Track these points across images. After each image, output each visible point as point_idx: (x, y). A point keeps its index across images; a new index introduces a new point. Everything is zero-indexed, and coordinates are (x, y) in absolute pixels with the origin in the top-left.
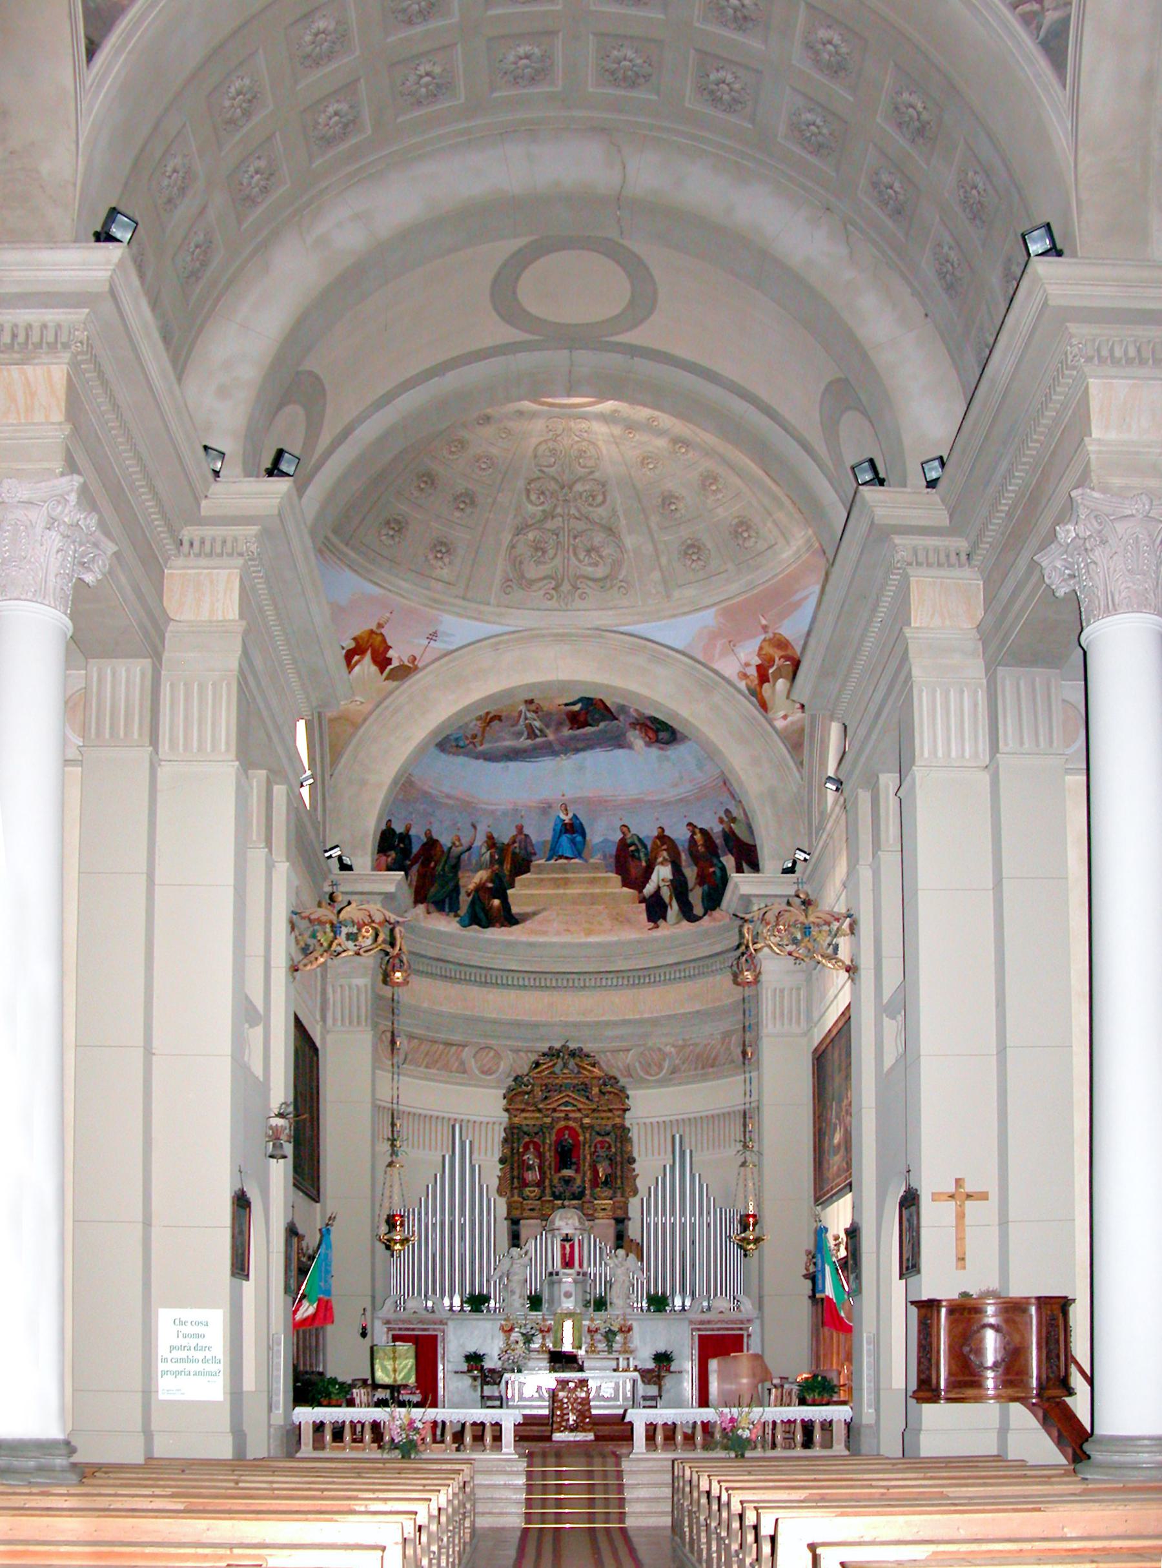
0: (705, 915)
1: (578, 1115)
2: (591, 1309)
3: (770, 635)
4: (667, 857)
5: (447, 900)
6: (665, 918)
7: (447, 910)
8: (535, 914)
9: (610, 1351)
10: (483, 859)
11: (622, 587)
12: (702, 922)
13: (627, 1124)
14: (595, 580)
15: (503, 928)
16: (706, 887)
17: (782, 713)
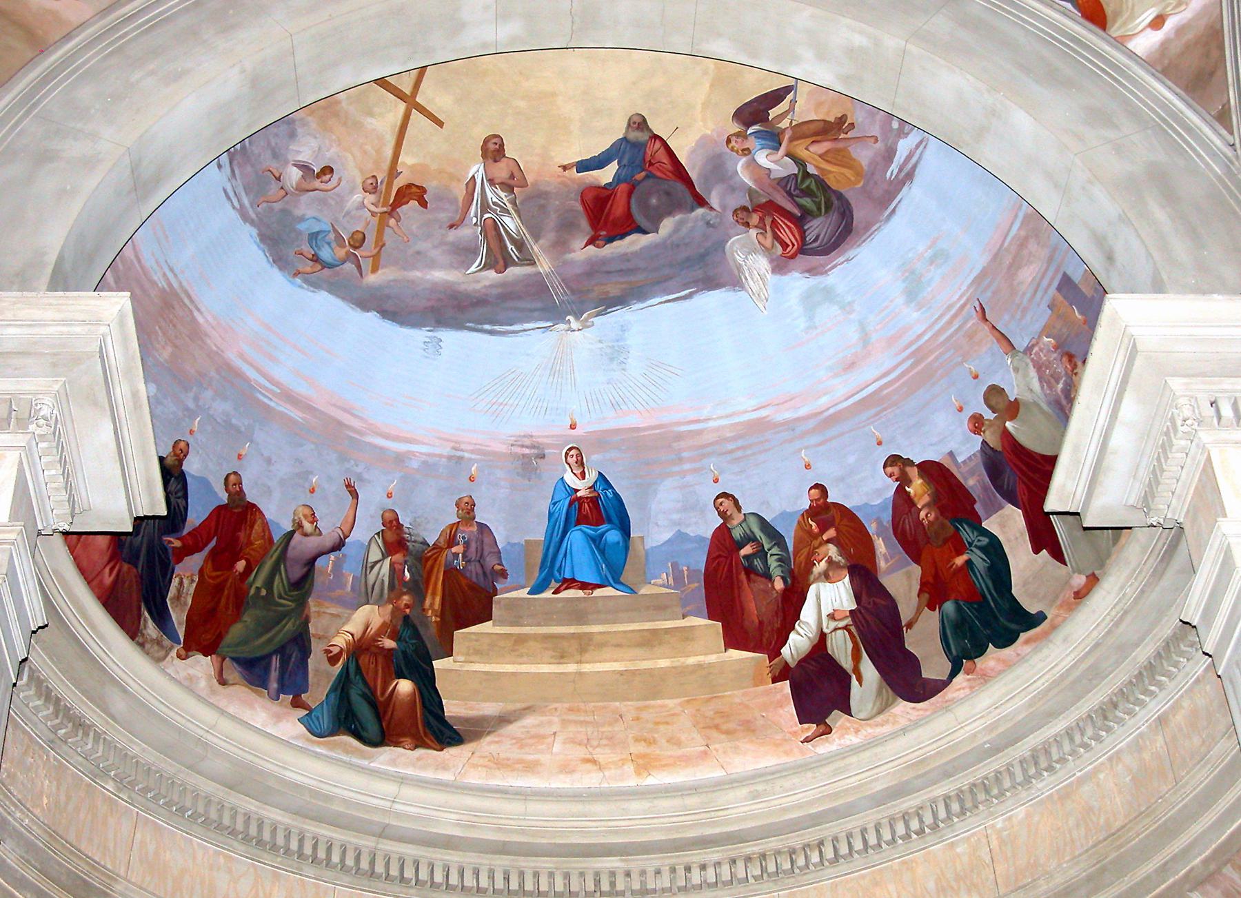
0: (954, 674)
5: (275, 662)
6: (847, 710)
7: (274, 685)
8: (504, 720)
10: (371, 577)
12: (949, 693)
15: (421, 752)
16: (949, 606)
17: (1150, 15)
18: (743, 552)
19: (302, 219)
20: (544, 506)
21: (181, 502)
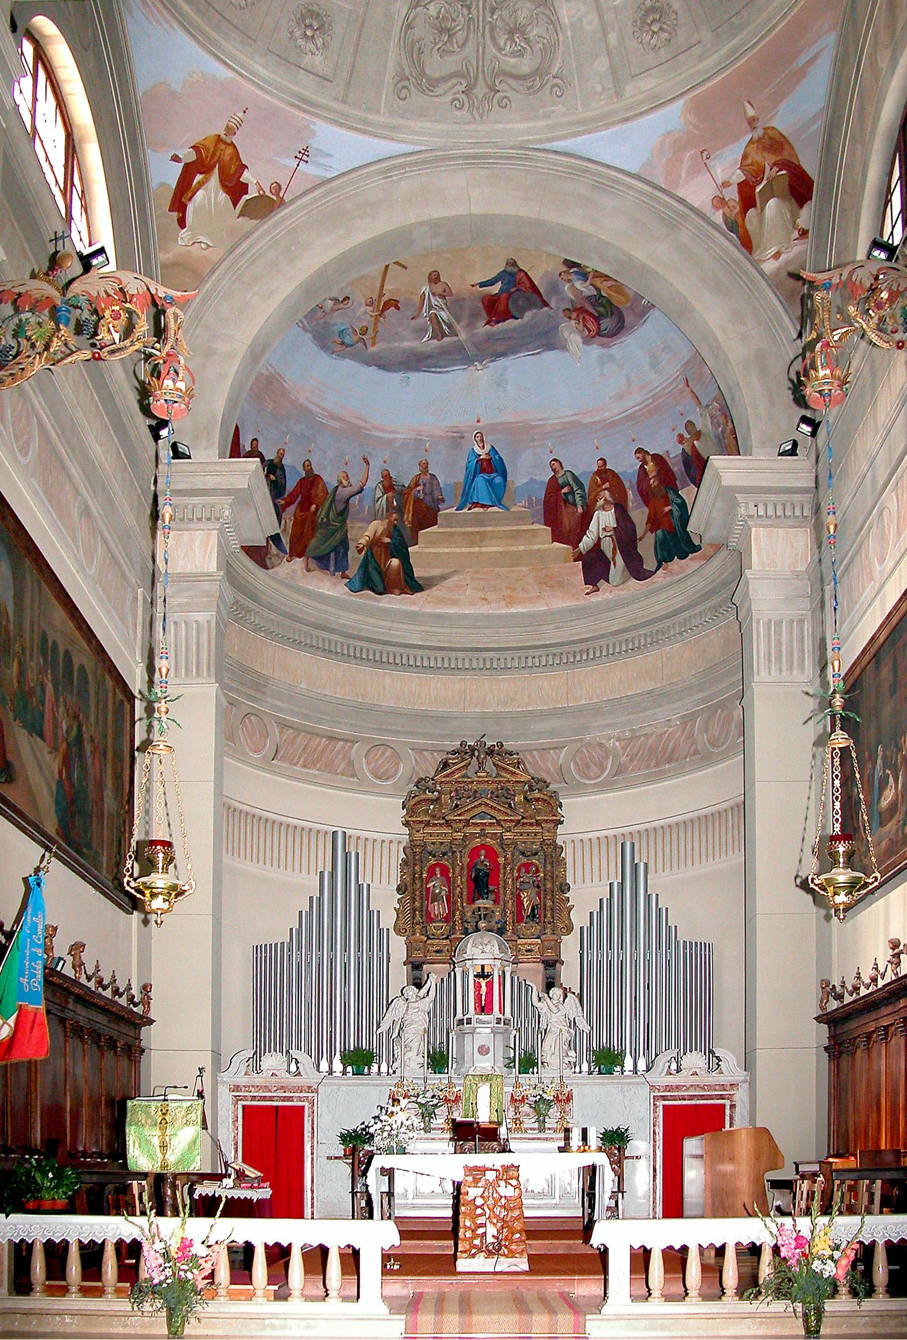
0: (658, 569)
1: (499, 830)
2: (515, 1071)
3: (759, 132)
4: (610, 499)
5: (332, 555)
8: (443, 578)
9: (542, 1129)
11: (556, 85)
13: (559, 841)
14: (517, 77)
16: (659, 532)
17: (773, 250)
18: (563, 491)
19: (335, 325)
20: (464, 463)
21: (283, 481)
